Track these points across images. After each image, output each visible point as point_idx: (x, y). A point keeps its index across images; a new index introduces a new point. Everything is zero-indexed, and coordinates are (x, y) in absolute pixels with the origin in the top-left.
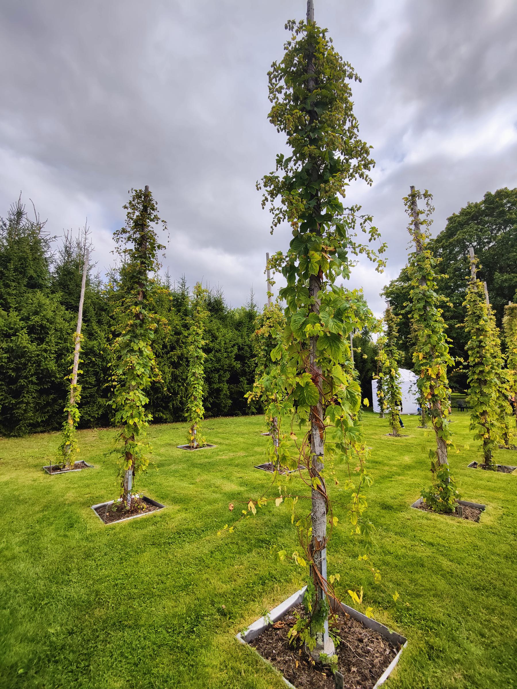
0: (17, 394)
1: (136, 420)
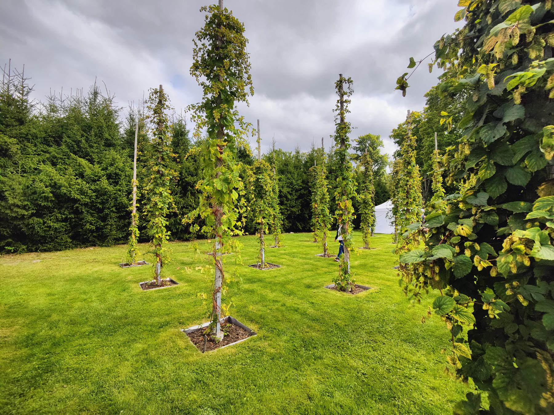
0: (104, 219)
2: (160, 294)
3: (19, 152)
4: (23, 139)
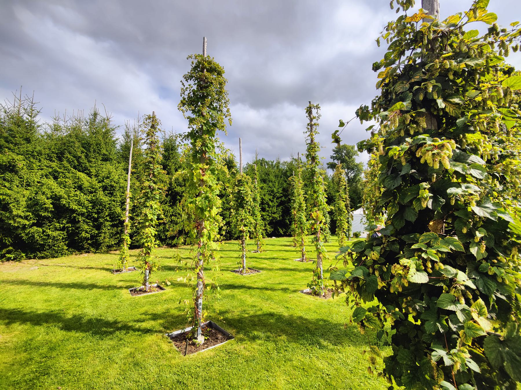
0: (98, 227)
1: (149, 244)
2: (148, 300)
3: (25, 167)
4: (29, 155)
